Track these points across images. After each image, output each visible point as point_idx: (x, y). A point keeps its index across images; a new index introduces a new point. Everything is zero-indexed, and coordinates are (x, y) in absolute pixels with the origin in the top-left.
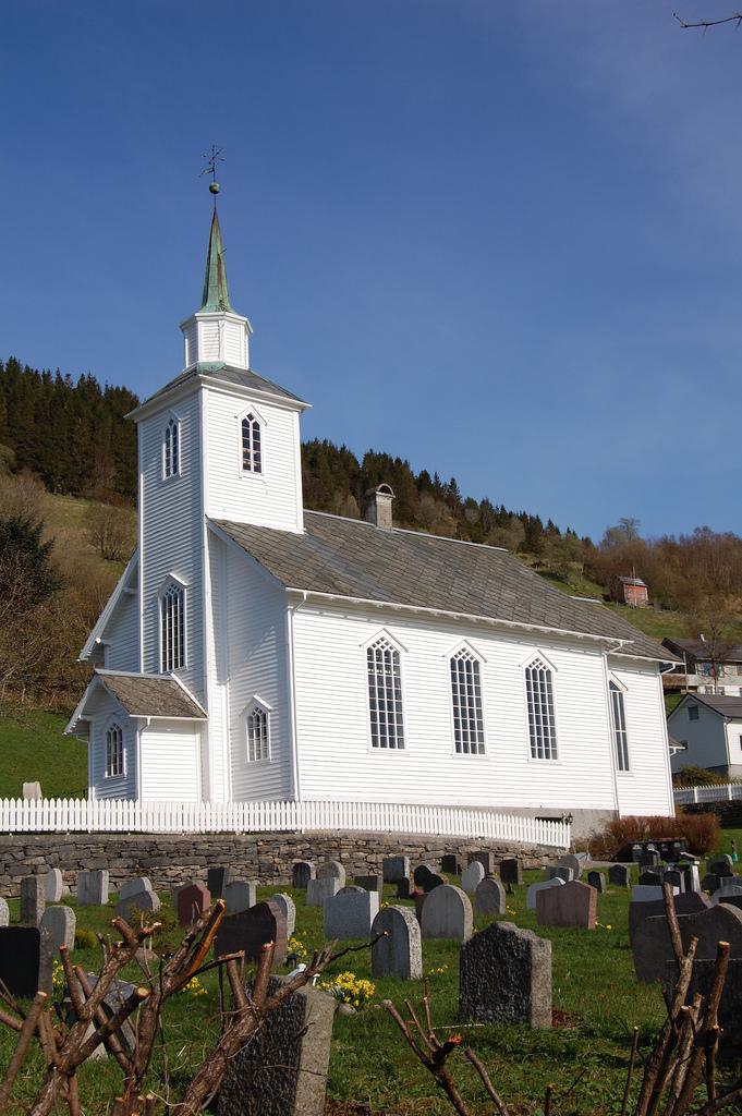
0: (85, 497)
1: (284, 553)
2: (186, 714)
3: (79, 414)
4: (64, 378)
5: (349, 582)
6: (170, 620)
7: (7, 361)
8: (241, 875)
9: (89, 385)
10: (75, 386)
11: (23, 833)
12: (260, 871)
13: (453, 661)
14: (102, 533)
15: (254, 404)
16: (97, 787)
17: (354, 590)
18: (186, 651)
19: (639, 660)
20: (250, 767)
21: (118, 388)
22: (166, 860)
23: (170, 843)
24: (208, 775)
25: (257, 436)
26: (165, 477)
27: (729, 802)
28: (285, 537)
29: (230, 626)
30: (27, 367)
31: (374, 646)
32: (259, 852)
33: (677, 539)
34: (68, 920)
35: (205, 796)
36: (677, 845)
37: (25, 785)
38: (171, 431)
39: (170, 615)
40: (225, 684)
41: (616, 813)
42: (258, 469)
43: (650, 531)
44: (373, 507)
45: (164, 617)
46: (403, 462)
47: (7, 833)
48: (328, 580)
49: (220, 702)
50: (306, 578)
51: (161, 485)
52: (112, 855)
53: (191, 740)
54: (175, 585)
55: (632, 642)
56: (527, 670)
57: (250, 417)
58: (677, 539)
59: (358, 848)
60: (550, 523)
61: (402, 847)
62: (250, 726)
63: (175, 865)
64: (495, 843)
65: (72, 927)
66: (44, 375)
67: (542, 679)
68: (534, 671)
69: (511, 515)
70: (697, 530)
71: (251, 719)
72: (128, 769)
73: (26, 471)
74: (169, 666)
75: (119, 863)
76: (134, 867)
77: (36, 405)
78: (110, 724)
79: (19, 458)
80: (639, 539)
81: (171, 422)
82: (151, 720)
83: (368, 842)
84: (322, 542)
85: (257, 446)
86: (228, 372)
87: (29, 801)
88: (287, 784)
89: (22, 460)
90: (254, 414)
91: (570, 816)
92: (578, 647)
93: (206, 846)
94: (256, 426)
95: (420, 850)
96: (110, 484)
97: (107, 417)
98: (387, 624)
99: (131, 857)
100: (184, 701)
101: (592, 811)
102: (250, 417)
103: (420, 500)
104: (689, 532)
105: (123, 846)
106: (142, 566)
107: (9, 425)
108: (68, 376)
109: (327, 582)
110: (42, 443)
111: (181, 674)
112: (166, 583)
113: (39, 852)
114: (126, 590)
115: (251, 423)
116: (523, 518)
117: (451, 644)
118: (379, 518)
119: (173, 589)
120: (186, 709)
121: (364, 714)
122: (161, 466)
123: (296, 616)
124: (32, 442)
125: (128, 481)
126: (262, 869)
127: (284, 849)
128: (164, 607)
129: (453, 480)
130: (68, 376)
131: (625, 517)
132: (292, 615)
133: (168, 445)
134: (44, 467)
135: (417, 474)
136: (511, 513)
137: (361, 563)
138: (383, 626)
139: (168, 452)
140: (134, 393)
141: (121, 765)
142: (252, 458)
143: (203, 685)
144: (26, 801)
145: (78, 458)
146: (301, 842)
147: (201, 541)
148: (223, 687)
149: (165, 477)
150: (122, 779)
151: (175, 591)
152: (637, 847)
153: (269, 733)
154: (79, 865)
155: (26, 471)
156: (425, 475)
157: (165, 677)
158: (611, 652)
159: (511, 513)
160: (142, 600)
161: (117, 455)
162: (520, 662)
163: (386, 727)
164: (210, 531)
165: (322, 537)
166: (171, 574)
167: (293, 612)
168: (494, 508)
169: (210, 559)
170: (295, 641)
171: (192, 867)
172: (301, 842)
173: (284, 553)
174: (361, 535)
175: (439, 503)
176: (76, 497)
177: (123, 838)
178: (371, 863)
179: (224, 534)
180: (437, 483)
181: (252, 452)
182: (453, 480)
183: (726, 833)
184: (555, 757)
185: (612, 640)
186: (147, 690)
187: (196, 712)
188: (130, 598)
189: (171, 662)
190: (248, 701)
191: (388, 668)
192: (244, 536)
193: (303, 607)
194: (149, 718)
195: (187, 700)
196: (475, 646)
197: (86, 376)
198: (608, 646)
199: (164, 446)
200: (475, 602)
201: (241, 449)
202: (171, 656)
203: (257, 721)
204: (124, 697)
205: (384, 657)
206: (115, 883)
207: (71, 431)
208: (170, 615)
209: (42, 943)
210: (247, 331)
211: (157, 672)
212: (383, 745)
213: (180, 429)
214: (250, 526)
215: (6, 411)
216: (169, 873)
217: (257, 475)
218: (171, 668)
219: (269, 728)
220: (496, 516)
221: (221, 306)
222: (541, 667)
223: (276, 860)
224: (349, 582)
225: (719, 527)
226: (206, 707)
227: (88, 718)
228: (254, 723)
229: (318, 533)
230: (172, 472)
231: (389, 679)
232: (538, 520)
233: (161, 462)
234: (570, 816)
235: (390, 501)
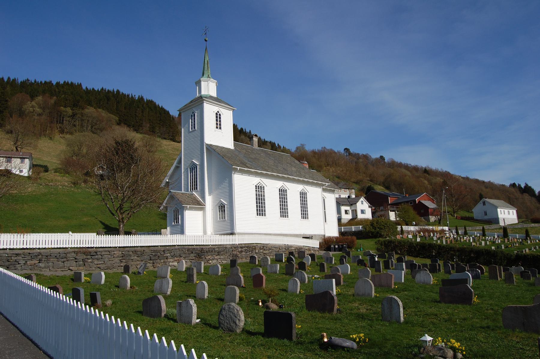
0: (140, 133)
1: (230, 155)
2: (199, 205)
3: (138, 107)
4: (133, 96)
5: (250, 164)
6: (192, 175)
7: (116, 90)
8: (227, 258)
9: (141, 99)
10: (137, 99)
11: (163, 246)
12: (233, 257)
13: (279, 189)
14: (147, 144)
15: (219, 108)
16: (170, 227)
17: (252, 167)
18: (198, 185)
19: (330, 189)
20: (219, 222)
21: (150, 100)
22: (206, 254)
23: (207, 248)
24: (206, 225)
25: (220, 118)
26: (191, 130)
27: (353, 231)
28: (229, 150)
29: (212, 176)
30: (122, 92)
31: (257, 184)
32: (233, 251)
33: (317, 150)
34: (237, 291)
35: (205, 232)
36: (345, 246)
37: (162, 230)
38: (193, 116)
39: (193, 173)
40: (211, 196)
41: (324, 235)
42: (220, 128)
43: (309, 148)
44: (252, 141)
45: (190, 174)
46: (236, 125)
47: (158, 246)
48: (244, 164)
49: (209, 201)
50: (238, 163)
51: (189, 132)
52: (190, 253)
53: (200, 213)
54: (194, 164)
55: (330, 184)
56: (300, 192)
57: (218, 112)
58: (317, 150)
59: (260, 248)
60: (278, 144)
61: (273, 248)
62: (219, 209)
63: (208, 255)
64: (299, 247)
65: (238, 294)
66: (127, 95)
67: (284, 192)
68: (302, 192)
69: (267, 141)
70: (322, 148)
71: (219, 207)
72: (181, 222)
73: (122, 124)
74: (192, 189)
75: (192, 255)
76: (196, 256)
77: (125, 104)
78: (174, 208)
79: (119, 120)
80: (306, 150)
81: (193, 113)
82: (189, 207)
83: (263, 247)
84: (239, 152)
85: (220, 121)
86: (211, 97)
87: (165, 235)
88: (232, 227)
89: (120, 121)
90: (219, 111)
91: (312, 237)
92: (310, 185)
93: (217, 249)
94: (220, 115)
95: (278, 249)
96: (148, 129)
97: (147, 108)
98: (261, 178)
99: (196, 253)
100: (198, 201)
101: (318, 235)
102: (218, 112)
103: (240, 136)
104: (320, 149)
105: (193, 250)
106: (183, 157)
107: (117, 110)
108: (135, 95)
109: (244, 165)
110: (127, 116)
111: (196, 192)
112: (191, 163)
113: (168, 252)
114: (177, 165)
115: (218, 114)
116: (270, 142)
117: (279, 184)
118: (254, 144)
119: (193, 165)
120: (199, 203)
121: (299, 213)
122: (189, 126)
123: (235, 175)
124: (124, 116)
125: (153, 128)
126: (234, 256)
127: (240, 250)
128: (190, 171)
129: (250, 131)
130: (135, 95)
131: (302, 143)
132: (234, 175)
133: (192, 120)
134: (127, 123)
135: (239, 129)
136: (267, 141)
137: (252, 158)
138: (260, 178)
139: (192, 122)
140: (155, 101)
141: (179, 221)
142: (219, 126)
143: (204, 196)
144: (162, 235)
145: (138, 121)
146: (244, 247)
147: (203, 150)
148: (210, 196)
149: (191, 130)
150: (179, 225)
151: (194, 166)
152: (332, 246)
153: (226, 211)
154: (180, 256)
155: (122, 124)
156: (242, 129)
157: (191, 193)
158: (324, 187)
159: (267, 141)
160: (183, 168)
161: (150, 120)
162: (254, 183)
163: (261, 210)
164: (206, 147)
165: (239, 150)
166: (193, 161)
167: (234, 174)
168: (262, 139)
169: (206, 156)
170: (235, 183)
171: (213, 256)
172: (244, 247)
173: (230, 155)
174: (250, 150)
175: (246, 137)
176: (137, 132)
177: (193, 247)
178: (264, 253)
179: (211, 149)
180: (245, 131)
181: (219, 123)
182: (250, 131)
183: (357, 240)
184: (308, 219)
185: (324, 183)
186: (187, 197)
187: (202, 204)
188: (178, 167)
189: (193, 188)
190: (219, 201)
191: (261, 191)
192: (217, 149)
193: (237, 172)
194: (188, 206)
195: (199, 200)
196: (286, 185)
197: (140, 96)
198: (323, 185)
199: (191, 120)
200: (285, 171)
201: (215, 122)
202: (193, 186)
203: (222, 208)
204: (180, 199)
205: (260, 188)
206: (191, 262)
207: (136, 112)
208: (193, 173)
209: (293, 319)
210: (216, 85)
211: (188, 191)
212: (260, 215)
213: (196, 115)
214: (218, 146)
215: (116, 106)
216: (207, 258)
217: (220, 130)
218: (193, 190)
219: (226, 210)
220: (263, 142)
221: (208, 77)
222: (284, 188)
223: (238, 253)
224: (250, 164)
225: (328, 147)
226: (205, 202)
227: (167, 206)
228: (221, 208)
229: (238, 149)
230: (193, 128)
231: (261, 195)
232: (275, 143)
233: (189, 125)
234: (312, 237)
235: (257, 139)
